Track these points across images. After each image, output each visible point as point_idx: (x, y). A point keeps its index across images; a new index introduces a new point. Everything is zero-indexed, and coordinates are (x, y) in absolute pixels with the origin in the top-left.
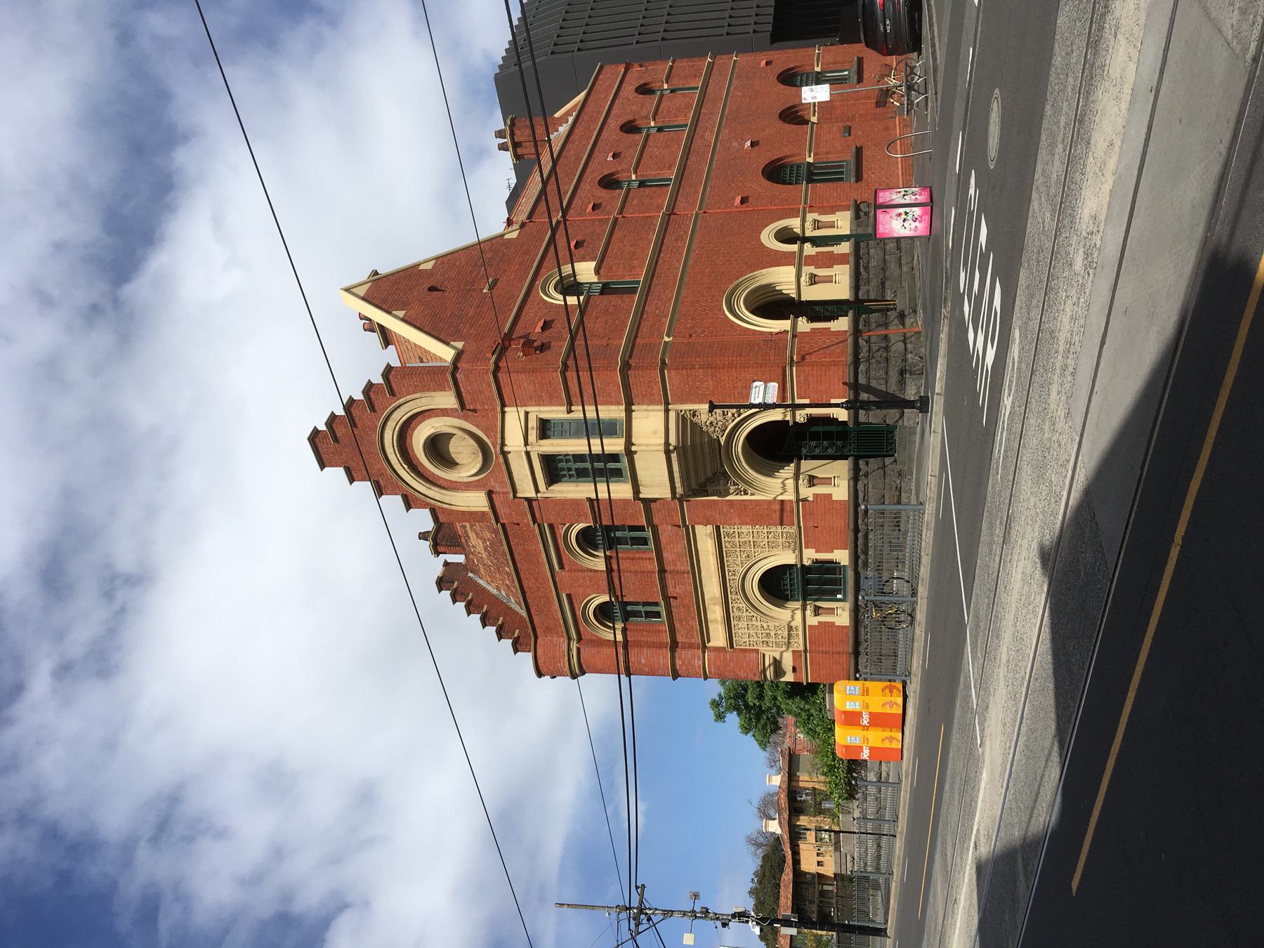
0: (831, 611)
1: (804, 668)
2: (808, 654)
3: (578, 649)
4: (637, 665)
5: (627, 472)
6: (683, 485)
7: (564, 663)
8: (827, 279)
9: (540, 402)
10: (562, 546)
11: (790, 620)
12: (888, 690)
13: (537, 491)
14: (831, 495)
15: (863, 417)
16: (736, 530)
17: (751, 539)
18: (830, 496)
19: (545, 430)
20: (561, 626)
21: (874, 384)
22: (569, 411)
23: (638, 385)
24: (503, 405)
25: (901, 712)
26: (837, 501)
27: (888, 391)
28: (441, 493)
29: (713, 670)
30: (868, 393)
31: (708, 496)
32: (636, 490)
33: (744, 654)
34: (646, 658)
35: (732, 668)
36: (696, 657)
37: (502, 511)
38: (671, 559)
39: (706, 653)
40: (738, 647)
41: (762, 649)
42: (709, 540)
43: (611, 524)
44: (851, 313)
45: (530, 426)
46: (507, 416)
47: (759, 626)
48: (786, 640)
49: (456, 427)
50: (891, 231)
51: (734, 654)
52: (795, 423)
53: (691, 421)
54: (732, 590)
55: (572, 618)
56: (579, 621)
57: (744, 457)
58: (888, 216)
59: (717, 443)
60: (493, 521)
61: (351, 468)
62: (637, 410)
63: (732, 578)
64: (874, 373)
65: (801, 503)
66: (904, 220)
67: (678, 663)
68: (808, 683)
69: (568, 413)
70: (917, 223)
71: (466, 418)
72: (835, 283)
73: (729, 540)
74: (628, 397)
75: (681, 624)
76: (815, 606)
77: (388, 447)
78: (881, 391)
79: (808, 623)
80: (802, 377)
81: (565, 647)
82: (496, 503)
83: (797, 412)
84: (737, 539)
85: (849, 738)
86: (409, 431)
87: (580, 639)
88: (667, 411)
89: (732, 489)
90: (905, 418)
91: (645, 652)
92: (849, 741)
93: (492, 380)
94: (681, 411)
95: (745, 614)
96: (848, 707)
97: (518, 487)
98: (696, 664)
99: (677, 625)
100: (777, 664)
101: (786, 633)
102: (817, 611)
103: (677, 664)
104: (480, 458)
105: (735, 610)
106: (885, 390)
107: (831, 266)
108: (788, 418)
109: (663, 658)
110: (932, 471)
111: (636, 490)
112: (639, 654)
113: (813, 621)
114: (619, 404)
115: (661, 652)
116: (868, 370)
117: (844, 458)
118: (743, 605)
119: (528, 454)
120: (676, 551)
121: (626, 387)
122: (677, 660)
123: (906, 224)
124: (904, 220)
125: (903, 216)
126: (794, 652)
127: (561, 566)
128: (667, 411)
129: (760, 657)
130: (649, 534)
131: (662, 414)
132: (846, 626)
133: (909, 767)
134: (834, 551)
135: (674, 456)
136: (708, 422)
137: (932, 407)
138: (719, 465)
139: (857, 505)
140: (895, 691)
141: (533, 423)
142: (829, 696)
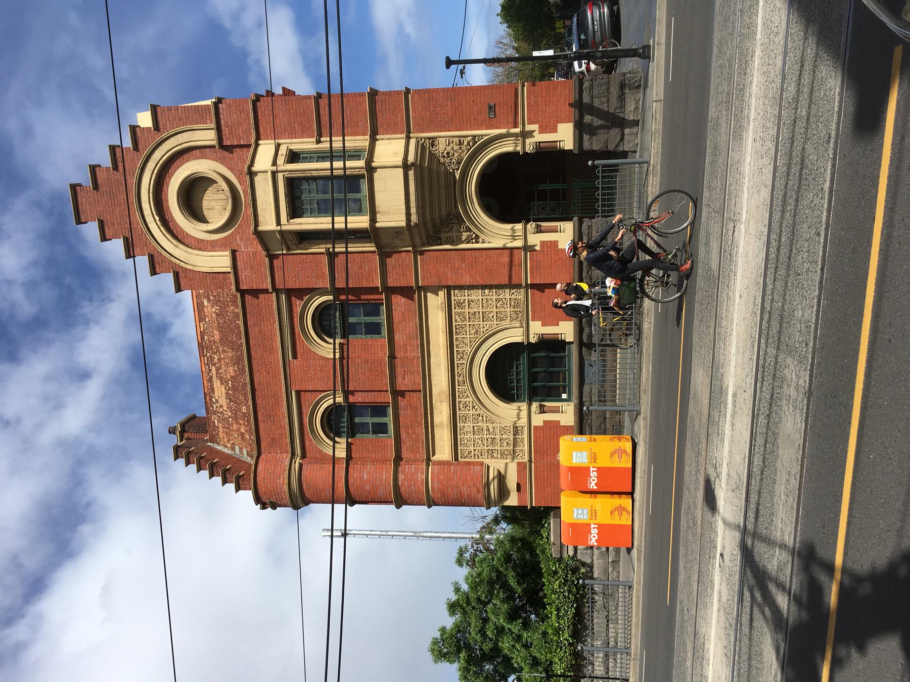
0: (556, 410)
2: (533, 464)
3: (301, 465)
4: (358, 482)
5: (366, 204)
6: (418, 213)
7: (284, 478)
8: (555, 409)
9: (293, 134)
10: (298, 329)
11: (516, 419)
12: (616, 513)
13: (278, 223)
14: (559, 421)
15: (587, 142)
17: (481, 310)
18: (558, 422)
19: (294, 157)
20: (286, 438)
21: (597, 103)
22: (318, 142)
23: (384, 112)
24: (258, 138)
25: (630, 465)
26: (564, 426)
27: (610, 111)
28: (186, 252)
29: (436, 486)
30: (591, 114)
31: (441, 244)
32: (373, 220)
33: (468, 467)
34: (369, 473)
35: (454, 482)
36: (420, 471)
37: (243, 275)
38: (402, 343)
39: (430, 467)
40: (463, 460)
41: (487, 461)
42: (440, 312)
43: (345, 287)
44: (575, 219)
45: (280, 153)
46: (260, 148)
47: (485, 428)
48: (511, 448)
49: (215, 171)
51: (459, 467)
52: (525, 153)
53: (430, 152)
54: (460, 379)
55: (301, 449)
56: (296, 324)
59: (452, 177)
60: (233, 287)
61: (105, 221)
62: (380, 139)
63: (460, 362)
64: (597, 90)
65: (528, 253)
67: (401, 477)
68: (532, 507)
69: (317, 144)
71: (221, 160)
72: (560, 232)
73: (460, 311)
74: (373, 126)
75: (407, 433)
76: (538, 225)
77: (148, 215)
78: (604, 110)
79: (534, 424)
81: (287, 462)
82: (239, 263)
83: (527, 140)
85: (575, 512)
86: (167, 178)
87: (304, 456)
88: (408, 138)
89: (465, 235)
90: (626, 142)
91: (368, 468)
92: (575, 516)
93: (251, 107)
94: (421, 140)
95: (471, 412)
96: (574, 461)
97: (261, 218)
98: (419, 479)
99: (403, 435)
100: (501, 478)
101: (512, 437)
102: (542, 410)
103: (400, 479)
104: (229, 207)
105: (461, 407)
106: (606, 109)
107: (557, 324)
108: (519, 148)
109: (386, 473)
110: (657, 95)
111: (373, 220)
112: (362, 470)
113: (538, 420)
114: (364, 134)
115: (384, 467)
116: (591, 88)
117: (570, 219)
118: (470, 399)
119: (274, 174)
120: (407, 332)
122: (400, 474)
126: (519, 464)
127: (295, 357)
128: (408, 138)
129: (485, 469)
130: (389, 420)
131: (402, 142)
132: (571, 426)
133: (641, 542)
134: (560, 323)
135: (411, 173)
136: (445, 152)
137: (653, 54)
140: (624, 513)
141: (283, 150)
142: (554, 522)
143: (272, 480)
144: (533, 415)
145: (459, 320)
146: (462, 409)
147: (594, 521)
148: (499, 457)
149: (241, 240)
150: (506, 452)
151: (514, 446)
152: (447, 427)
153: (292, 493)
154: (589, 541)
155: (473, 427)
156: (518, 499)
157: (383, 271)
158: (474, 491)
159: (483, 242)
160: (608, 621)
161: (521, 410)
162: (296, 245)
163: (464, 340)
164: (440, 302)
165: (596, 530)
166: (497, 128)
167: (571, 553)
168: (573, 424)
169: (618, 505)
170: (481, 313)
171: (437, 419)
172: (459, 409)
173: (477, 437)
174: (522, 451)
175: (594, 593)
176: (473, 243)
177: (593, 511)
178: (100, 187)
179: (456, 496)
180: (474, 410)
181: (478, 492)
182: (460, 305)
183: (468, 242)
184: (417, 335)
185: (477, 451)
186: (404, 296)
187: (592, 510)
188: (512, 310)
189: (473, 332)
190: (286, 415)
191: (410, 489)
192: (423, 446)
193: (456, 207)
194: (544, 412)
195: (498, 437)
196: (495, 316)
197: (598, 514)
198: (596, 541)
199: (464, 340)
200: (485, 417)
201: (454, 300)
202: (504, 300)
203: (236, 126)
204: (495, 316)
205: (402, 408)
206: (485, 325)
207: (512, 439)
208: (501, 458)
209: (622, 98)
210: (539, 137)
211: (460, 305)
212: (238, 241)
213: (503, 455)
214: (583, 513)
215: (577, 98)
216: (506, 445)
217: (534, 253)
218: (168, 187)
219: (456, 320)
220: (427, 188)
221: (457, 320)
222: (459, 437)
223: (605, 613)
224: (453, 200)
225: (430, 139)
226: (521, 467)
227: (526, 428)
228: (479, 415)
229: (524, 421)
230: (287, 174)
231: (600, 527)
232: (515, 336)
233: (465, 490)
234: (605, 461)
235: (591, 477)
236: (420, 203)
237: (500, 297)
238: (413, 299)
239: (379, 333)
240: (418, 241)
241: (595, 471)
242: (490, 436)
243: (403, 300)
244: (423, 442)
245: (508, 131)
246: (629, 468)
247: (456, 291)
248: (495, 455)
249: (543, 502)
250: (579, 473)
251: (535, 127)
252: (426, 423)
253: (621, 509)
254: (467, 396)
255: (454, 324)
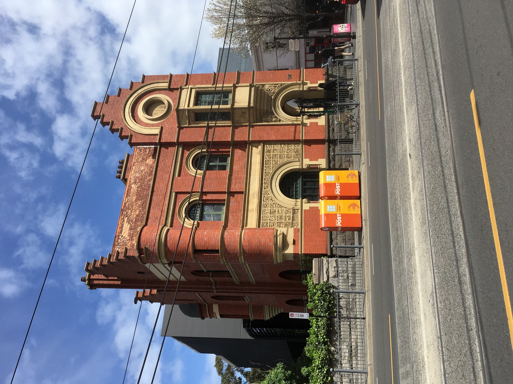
1: (300, 241)
3: (168, 230)
4: (201, 236)
6: (254, 103)
10: (184, 164)
12: (352, 207)
16: (272, 148)
17: (279, 154)
25: (358, 182)
29: (246, 238)
37: (163, 136)
39: (243, 231)
42: (258, 155)
47: (277, 211)
50: (338, 30)
51: (260, 230)
56: (183, 162)
57: (282, 98)
58: (337, 27)
66: (342, 28)
70: (346, 28)
75: (233, 216)
79: (304, 208)
80: (307, 72)
84: (272, 154)
86: (141, 101)
87: (171, 226)
98: (236, 234)
99: (230, 217)
100: (284, 237)
101: (291, 215)
105: (265, 199)
120: (240, 165)
121: (233, 136)
123: (343, 29)
124: (342, 28)
125: (342, 27)
126: (295, 229)
127: (179, 175)
135: (253, 89)
138: (270, 108)
139: (329, 127)
140: (356, 207)
143: (150, 234)
144: (303, 204)
145: (267, 158)
146: (265, 200)
147: (339, 212)
148: (284, 226)
149: (167, 123)
150: (288, 223)
151: (292, 220)
152: (256, 210)
153: (160, 241)
154: (336, 224)
155: (270, 210)
156: (294, 249)
157: (233, 134)
158: (268, 240)
159: (283, 122)
160: (350, 329)
161: (297, 202)
162: (193, 121)
163: (269, 167)
164: (259, 151)
165: (340, 217)
166: (291, 81)
167: (325, 279)
168: (325, 124)
169: (352, 203)
170: (279, 155)
171: (250, 207)
172: (264, 200)
173: (272, 215)
174: (297, 223)
175: (340, 307)
176: (277, 122)
177: (338, 207)
178: (109, 104)
179: (257, 244)
180: (271, 201)
181: (270, 242)
182: (269, 151)
183: (276, 122)
184: (245, 167)
185: (271, 223)
186: (241, 150)
187: (337, 206)
188: (295, 153)
189: (274, 163)
190: (166, 211)
191: (230, 240)
192: (241, 222)
193: (271, 109)
194: (310, 203)
195: (284, 215)
196: (286, 157)
197: (341, 208)
198: (340, 192)
199: (269, 167)
200: (277, 205)
201: (266, 149)
202: (291, 149)
203: (178, 82)
204: (286, 157)
205: (232, 202)
206: (281, 160)
207: (291, 217)
208: (285, 227)
209: (345, 71)
210: (309, 85)
211: (269, 151)
212: (166, 124)
213: (286, 225)
214: (333, 208)
215: (326, 72)
216: (288, 220)
217: (307, 127)
218: (140, 104)
219: (266, 158)
220: (259, 97)
221: (266, 158)
222: (262, 215)
223: (349, 323)
224: (270, 106)
225: (262, 85)
226: (296, 231)
227: (300, 210)
228: (274, 204)
229: (299, 207)
230: (197, 90)
231: (343, 215)
232: (296, 166)
233: (263, 240)
234: (344, 180)
235: (336, 189)
236: (255, 100)
237: (289, 148)
238: (245, 151)
239: (226, 170)
240: (252, 121)
241: (340, 216)
242: (279, 215)
243: (240, 151)
244: (241, 220)
245: (296, 82)
246: (357, 183)
247: (267, 146)
248: (281, 225)
249: (308, 251)
250: (330, 186)
251: (308, 82)
252: (244, 207)
253: (354, 205)
254: (268, 194)
255: (265, 159)
